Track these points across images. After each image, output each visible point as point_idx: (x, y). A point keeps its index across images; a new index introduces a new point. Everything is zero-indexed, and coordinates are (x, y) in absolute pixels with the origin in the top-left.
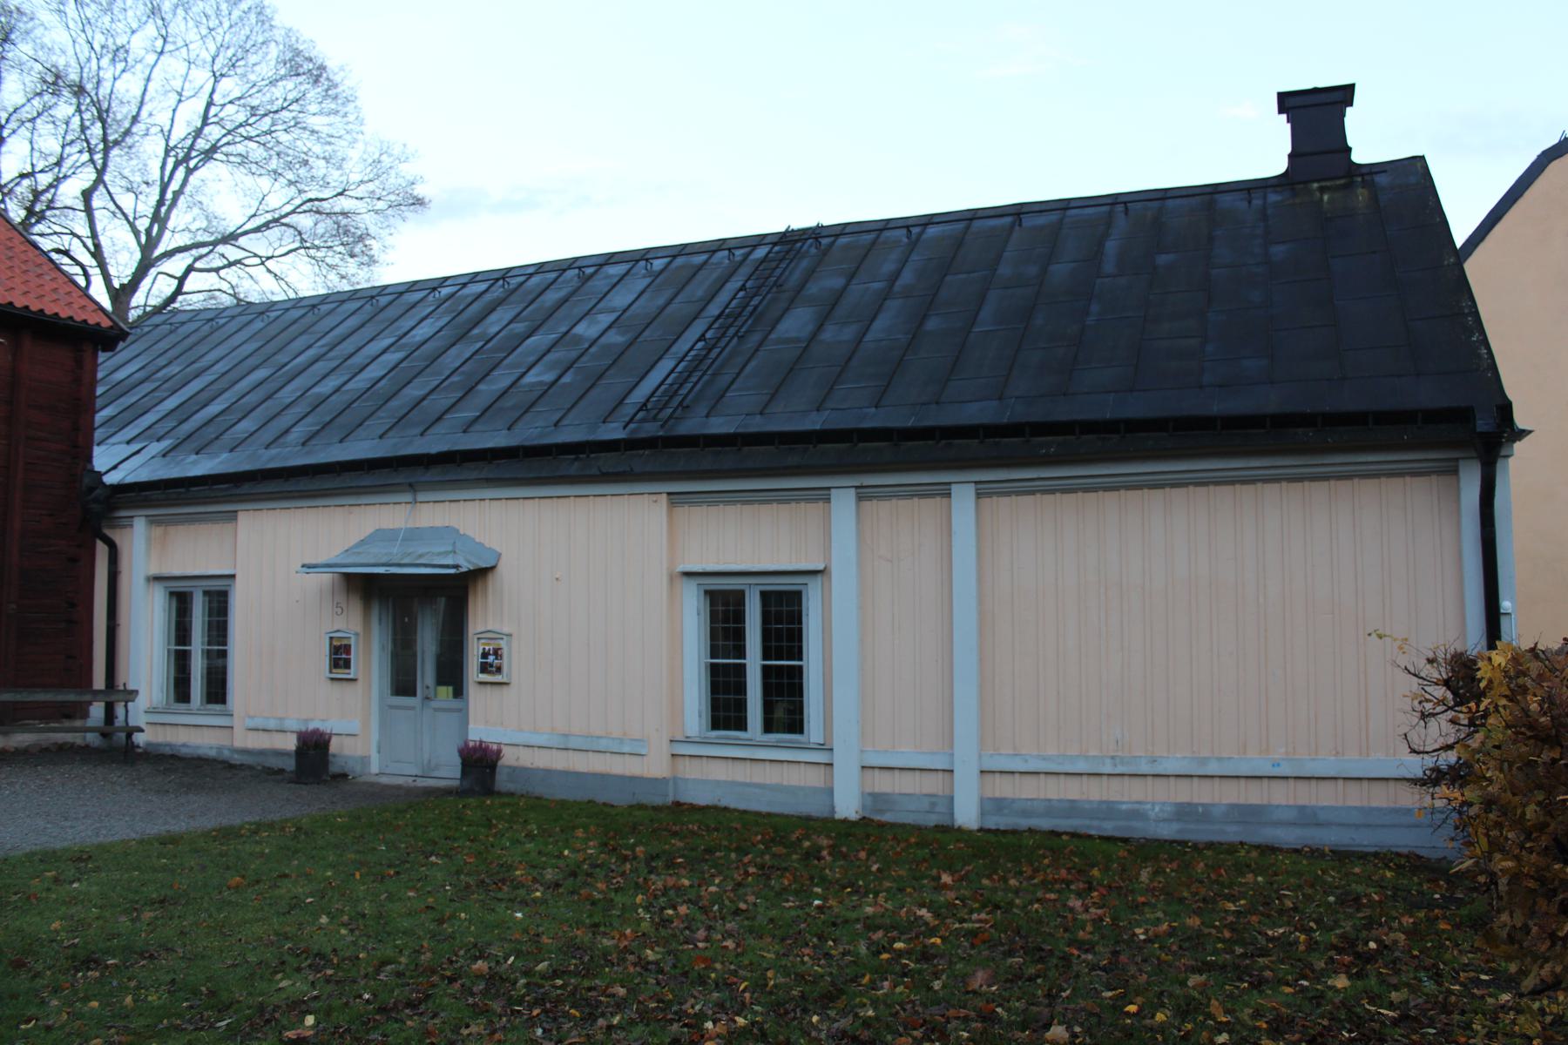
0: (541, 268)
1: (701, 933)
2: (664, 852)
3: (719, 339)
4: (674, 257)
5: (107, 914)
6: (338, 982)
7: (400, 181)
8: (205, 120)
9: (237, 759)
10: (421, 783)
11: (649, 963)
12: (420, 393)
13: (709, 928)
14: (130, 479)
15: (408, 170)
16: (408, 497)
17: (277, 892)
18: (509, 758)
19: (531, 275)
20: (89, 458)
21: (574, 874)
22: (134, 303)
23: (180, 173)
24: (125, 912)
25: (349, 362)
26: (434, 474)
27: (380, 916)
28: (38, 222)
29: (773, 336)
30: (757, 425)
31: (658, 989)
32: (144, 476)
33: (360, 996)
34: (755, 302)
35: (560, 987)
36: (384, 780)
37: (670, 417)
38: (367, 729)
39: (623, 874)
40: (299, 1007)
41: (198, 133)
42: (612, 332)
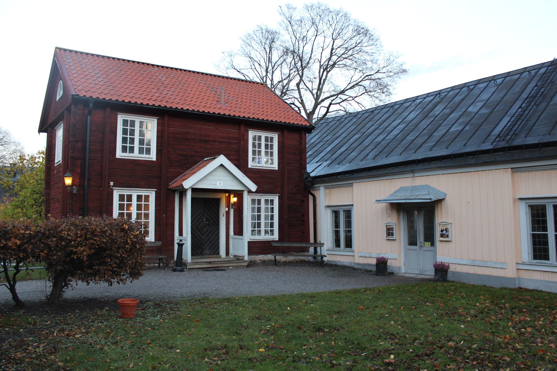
0: (453, 88)
1: (539, 340)
2: (517, 306)
3: (528, 107)
4: (506, 77)
5: (323, 315)
6: (400, 345)
7: (397, 64)
8: (331, 56)
9: (356, 267)
10: (420, 276)
11: (518, 349)
12: (413, 138)
13: (542, 338)
14: (318, 175)
15: (400, 61)
16: (411, 175)
17: (375, 312)
18: (452, 268)
19: (449, 91)
20: (306, 168)
21: (482, 313)
22: (314, 117)
23: (325, 73)
24: (328, 315)
25: (387, 129)
26: (420, 166)
27: (412, 323)
28: (285, 95)
29: (551, 103)
30: (548, 139)
31: (524, 360)
32: (322, 173)
33: (409, 350)
34: (542, 90)
35: (483, 355)
36: (407, 275)
37: (510, 139)
38: (402, 259)
39: (501, 314)
40: (388, 352)
41: (330, 59)
42: (483, 109)
